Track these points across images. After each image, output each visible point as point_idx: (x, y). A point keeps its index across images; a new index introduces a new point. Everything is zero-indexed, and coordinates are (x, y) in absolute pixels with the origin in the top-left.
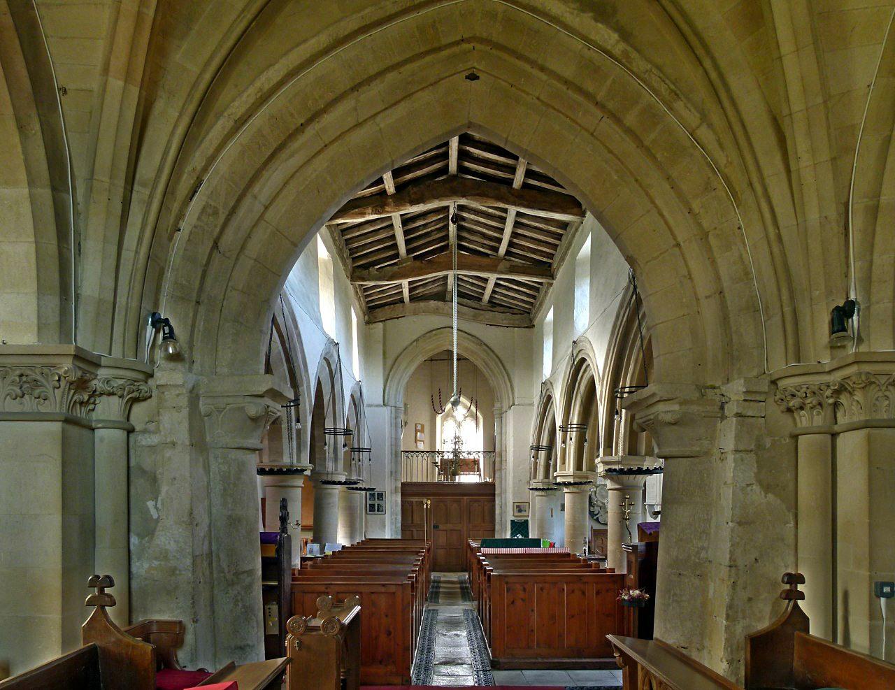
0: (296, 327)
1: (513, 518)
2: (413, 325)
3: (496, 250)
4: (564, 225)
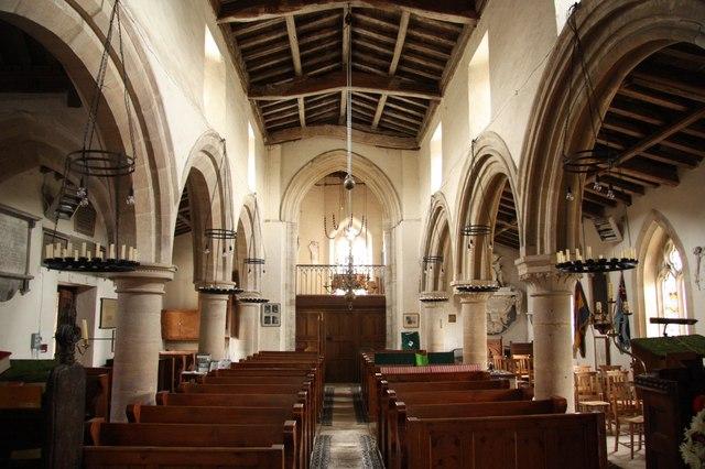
0: (157, 91)
1: (405, 331)
2: (312, 146)
3: (386, 69)
4: (427, 102)
